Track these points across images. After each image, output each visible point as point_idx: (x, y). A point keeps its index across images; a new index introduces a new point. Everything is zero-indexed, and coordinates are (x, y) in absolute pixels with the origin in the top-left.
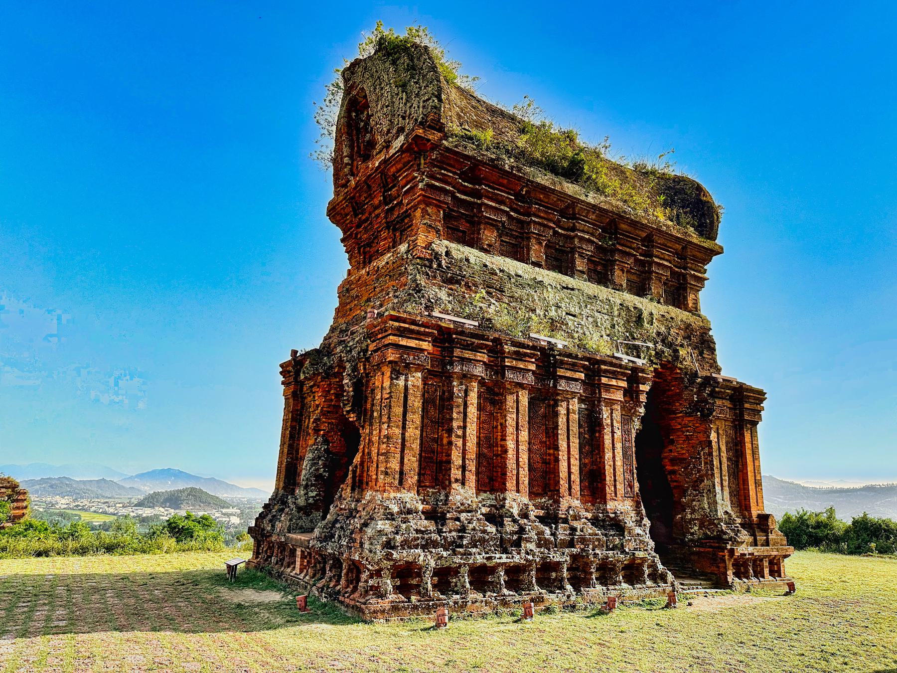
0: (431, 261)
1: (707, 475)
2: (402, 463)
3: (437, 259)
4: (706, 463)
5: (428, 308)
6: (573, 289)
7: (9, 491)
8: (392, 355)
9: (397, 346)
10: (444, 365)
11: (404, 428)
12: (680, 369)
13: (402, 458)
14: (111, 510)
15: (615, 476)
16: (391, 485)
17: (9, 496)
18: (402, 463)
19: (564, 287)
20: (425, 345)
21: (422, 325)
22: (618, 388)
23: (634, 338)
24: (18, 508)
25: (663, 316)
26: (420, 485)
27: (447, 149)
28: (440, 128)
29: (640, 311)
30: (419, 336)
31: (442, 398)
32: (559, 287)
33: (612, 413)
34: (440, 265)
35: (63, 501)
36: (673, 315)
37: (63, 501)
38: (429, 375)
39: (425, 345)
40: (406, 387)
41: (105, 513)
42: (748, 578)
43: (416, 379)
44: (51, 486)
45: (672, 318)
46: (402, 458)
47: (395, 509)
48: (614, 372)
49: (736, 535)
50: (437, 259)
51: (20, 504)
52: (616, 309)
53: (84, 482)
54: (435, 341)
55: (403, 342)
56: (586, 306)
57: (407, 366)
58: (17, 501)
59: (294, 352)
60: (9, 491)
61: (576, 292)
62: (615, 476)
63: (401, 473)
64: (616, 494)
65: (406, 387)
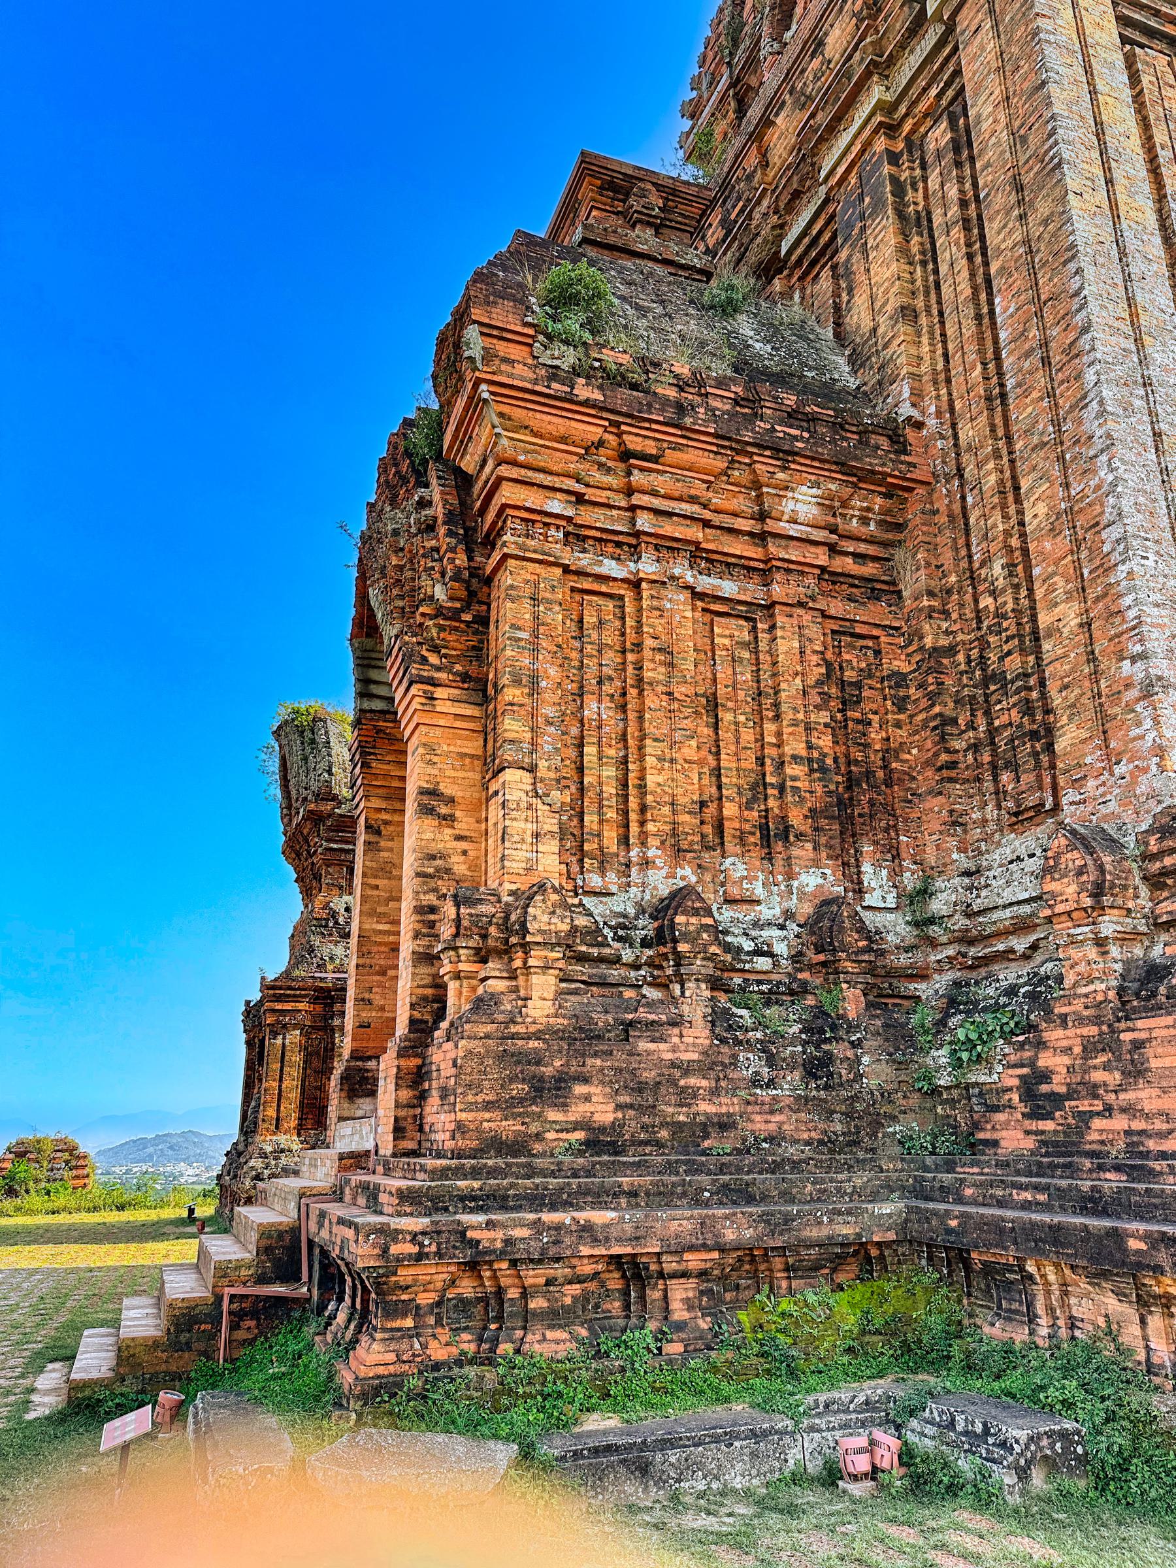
0: (327, 920)
2: (278, 1111)
3: (333, 917)
5: (321, 967)
7: (66, 1156)
8: (270, 1019)
9: (274, 1011)
10: (326, 1020)
11: (281, 1080)
13: (279, 1106)
16: (267, 1130)
17: (67, 1162)
18: (278, 1111)
20: (301, 1006)
21: (299, 989)
24: (77, 1177)
26: (299, 1130)
27: (341, 816)
28: (334, 798)
30: (296, 998)
31: (326, 1049)
34: (336, 923)
35: (191, 1172)
37: (191, 1172)
38: (306, 1032)
39: (301, 1006)
40: (284, 1045)
43: (294, 1036)
46: (279, 1106)
47: (269, 1149)
50: (333, 917)
51: (80, 1172)
54: (314, 1001)
55: (279, 1006)
57: (284, 1026)
58: (77, 1167)
59: (248, 1003)
60: (66, 1156)
63: (278, 1119)
65: (284, 1045)
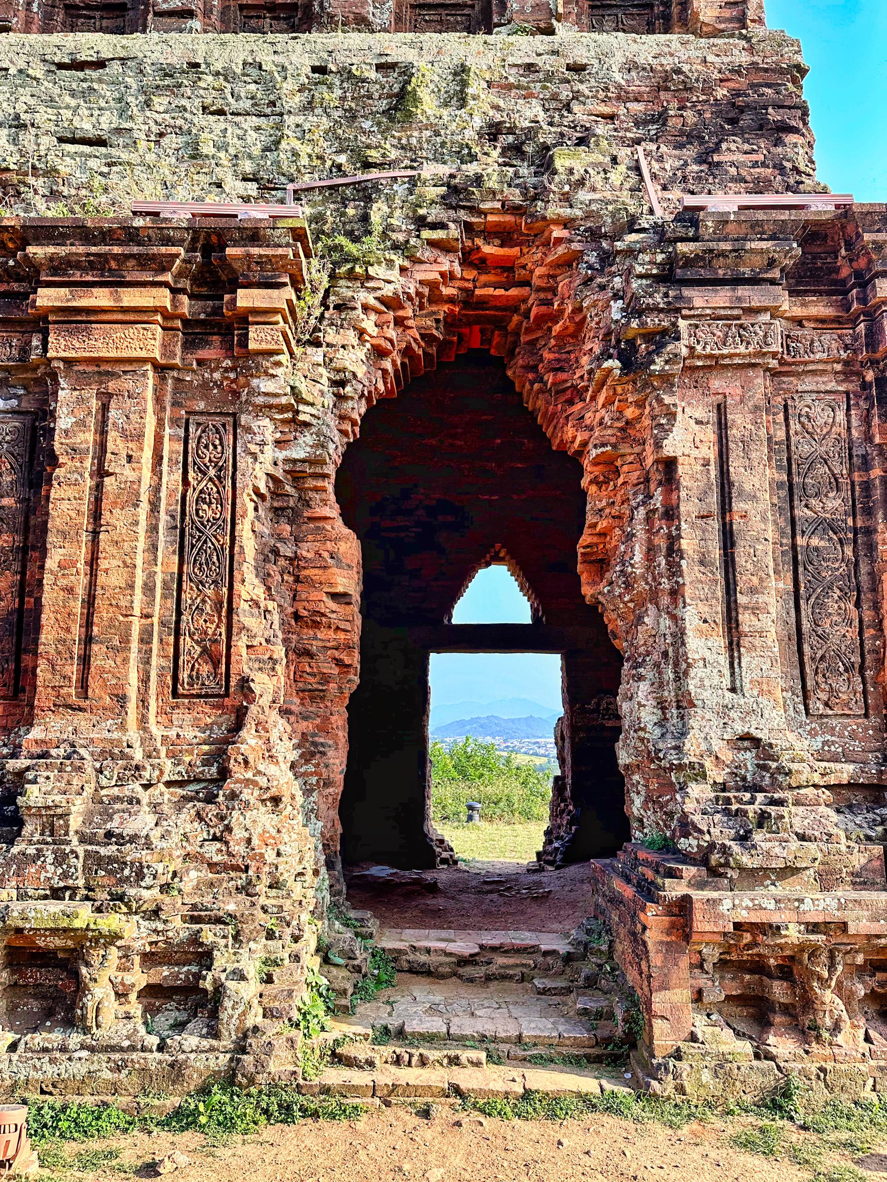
1: (654, 596)
4: (651, 552)
6: (100, 64)
12: (567, 223)
14: (542, 751)
15: (88, 624)
19: (61, 66)
22: (136, 316)
23: (367, 165)
25: (530, 68)
29: (406, 72)
32: (38, 70)
33: (105, 408)
36: (580, 55)
41: (536, 754)
42: (807, 1032)
44: (481, 726)
45: (577, 68)
48: (98, 263)
49: (743, 838)
52: (289, 86)
53: (513, 721)
56: (148, 104)
61: (115, 68)
62: (88, 624)
64: (84, 685)
